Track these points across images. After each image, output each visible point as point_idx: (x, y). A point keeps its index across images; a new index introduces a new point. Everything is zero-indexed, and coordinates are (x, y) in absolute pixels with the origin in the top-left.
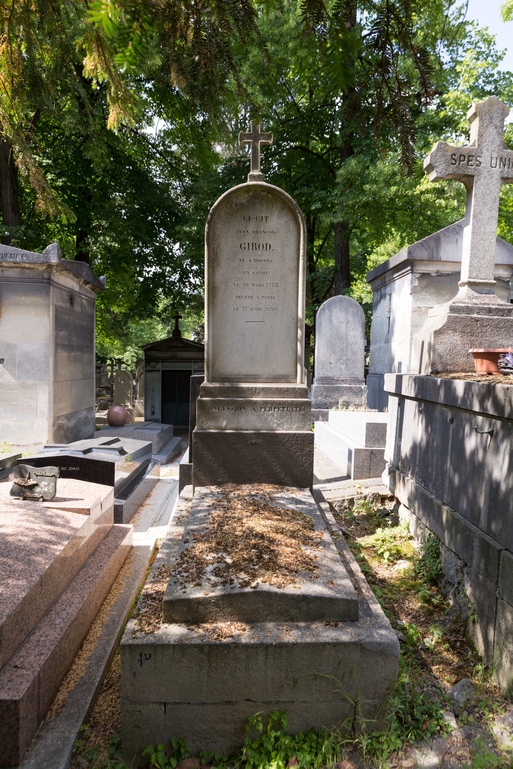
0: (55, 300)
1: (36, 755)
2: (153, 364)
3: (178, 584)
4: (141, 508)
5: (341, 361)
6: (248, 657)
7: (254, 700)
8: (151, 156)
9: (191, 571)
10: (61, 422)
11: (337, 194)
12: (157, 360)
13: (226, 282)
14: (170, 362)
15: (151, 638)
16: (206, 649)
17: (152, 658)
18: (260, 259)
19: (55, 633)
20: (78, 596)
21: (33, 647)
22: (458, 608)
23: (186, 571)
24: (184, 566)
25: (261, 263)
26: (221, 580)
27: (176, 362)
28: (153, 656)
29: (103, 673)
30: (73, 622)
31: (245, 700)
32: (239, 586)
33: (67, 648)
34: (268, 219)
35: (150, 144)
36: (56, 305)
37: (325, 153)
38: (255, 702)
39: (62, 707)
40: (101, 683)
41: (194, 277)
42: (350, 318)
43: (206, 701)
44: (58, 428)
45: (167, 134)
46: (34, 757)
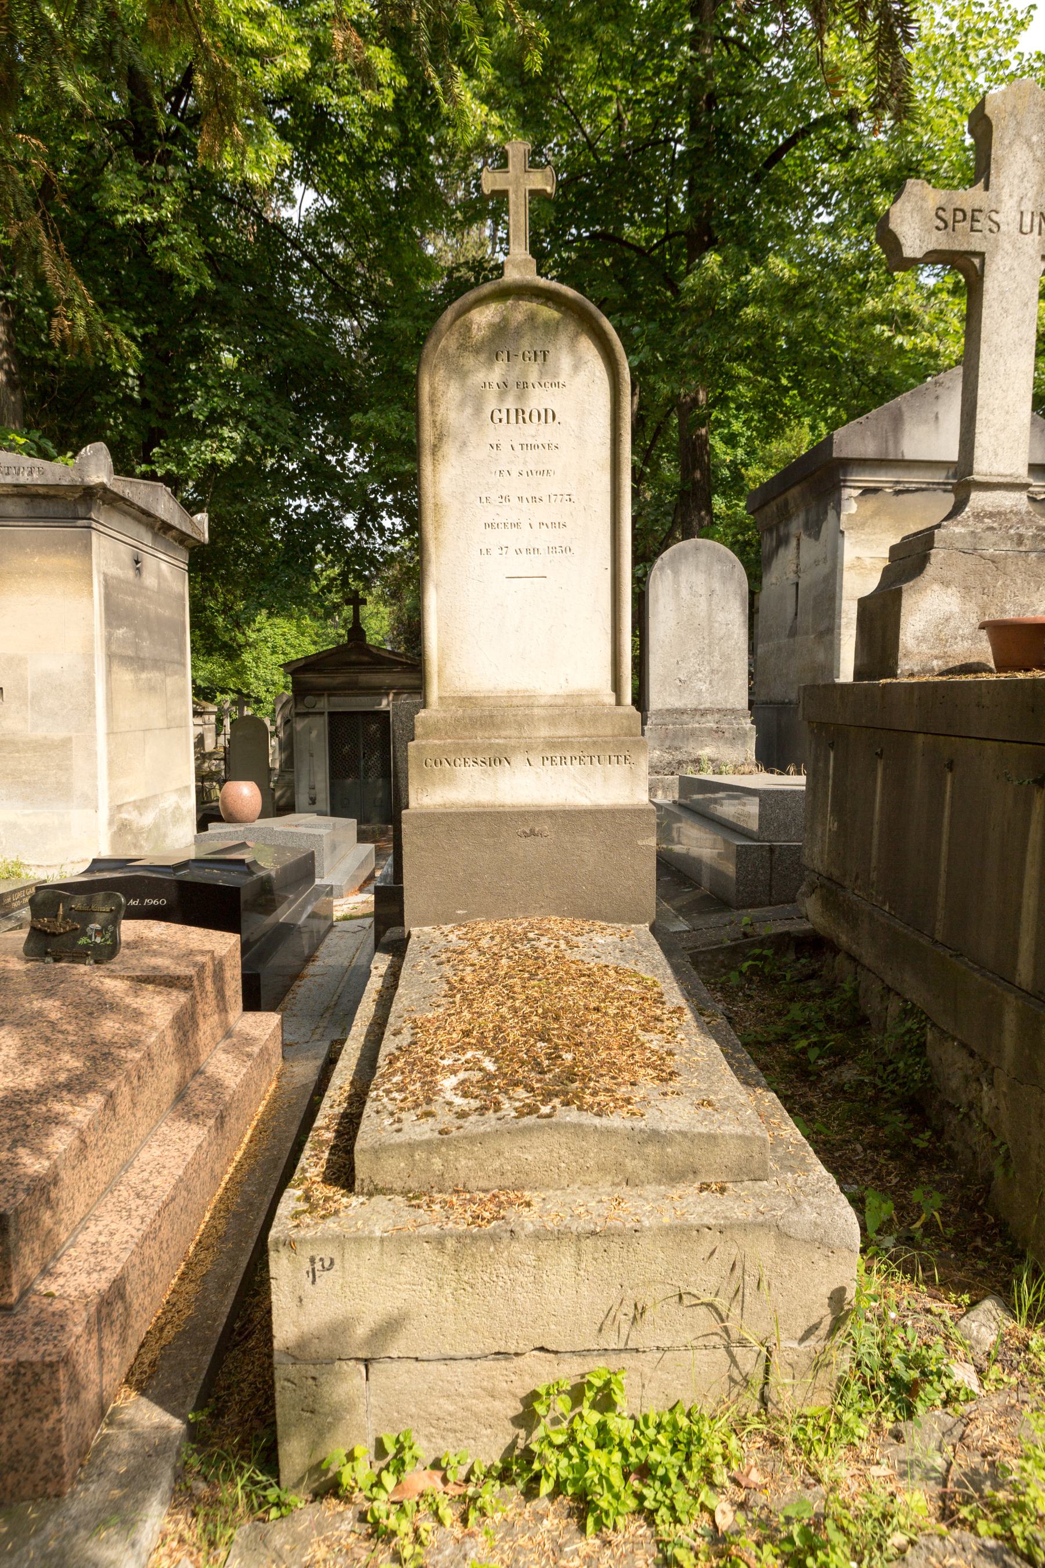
0: (103, 562)
1: (99, 1475)
2: (309, 699)
3: (385, 1115)
4: (298, 983)
5: (700, 675)
6: (539, 1259)
7: (554, 1348)
8: (292, 266)
9: (411, 1088)
10: (124, 816)
11: (683, 332)
12: (319, 691)
13: (463, 495)
14: (345, 695)
15: (332, 1225)
16: (449, 1245)
17: (336, 1267)
18: (534, 442)
19: (130, 1227)
20: (176, 1154)
21: (85, 1256)
22: (970, 1155)
23: (400, 1091)
24: (395, 1079)
25: (535, 452)
26: (475, 1104)
27: (357, 695)
28: (337, 1261)
29: (233, 1308)
30: (166, 1205)
31: (536, 1349)
32: (514, 1114)
33: (155, 1257)
34: (549, 357)
35: (289, 240)
36: (105, 575)
37: (656, 246)
38: (556, 1352)
39: (150, 1377)
40: (228, 1327)
41: (390, 515)
42: (717, 586)
43: (452, 1354)
44: (120, 829)
45: (327, 220)
46: (95, 1477)
